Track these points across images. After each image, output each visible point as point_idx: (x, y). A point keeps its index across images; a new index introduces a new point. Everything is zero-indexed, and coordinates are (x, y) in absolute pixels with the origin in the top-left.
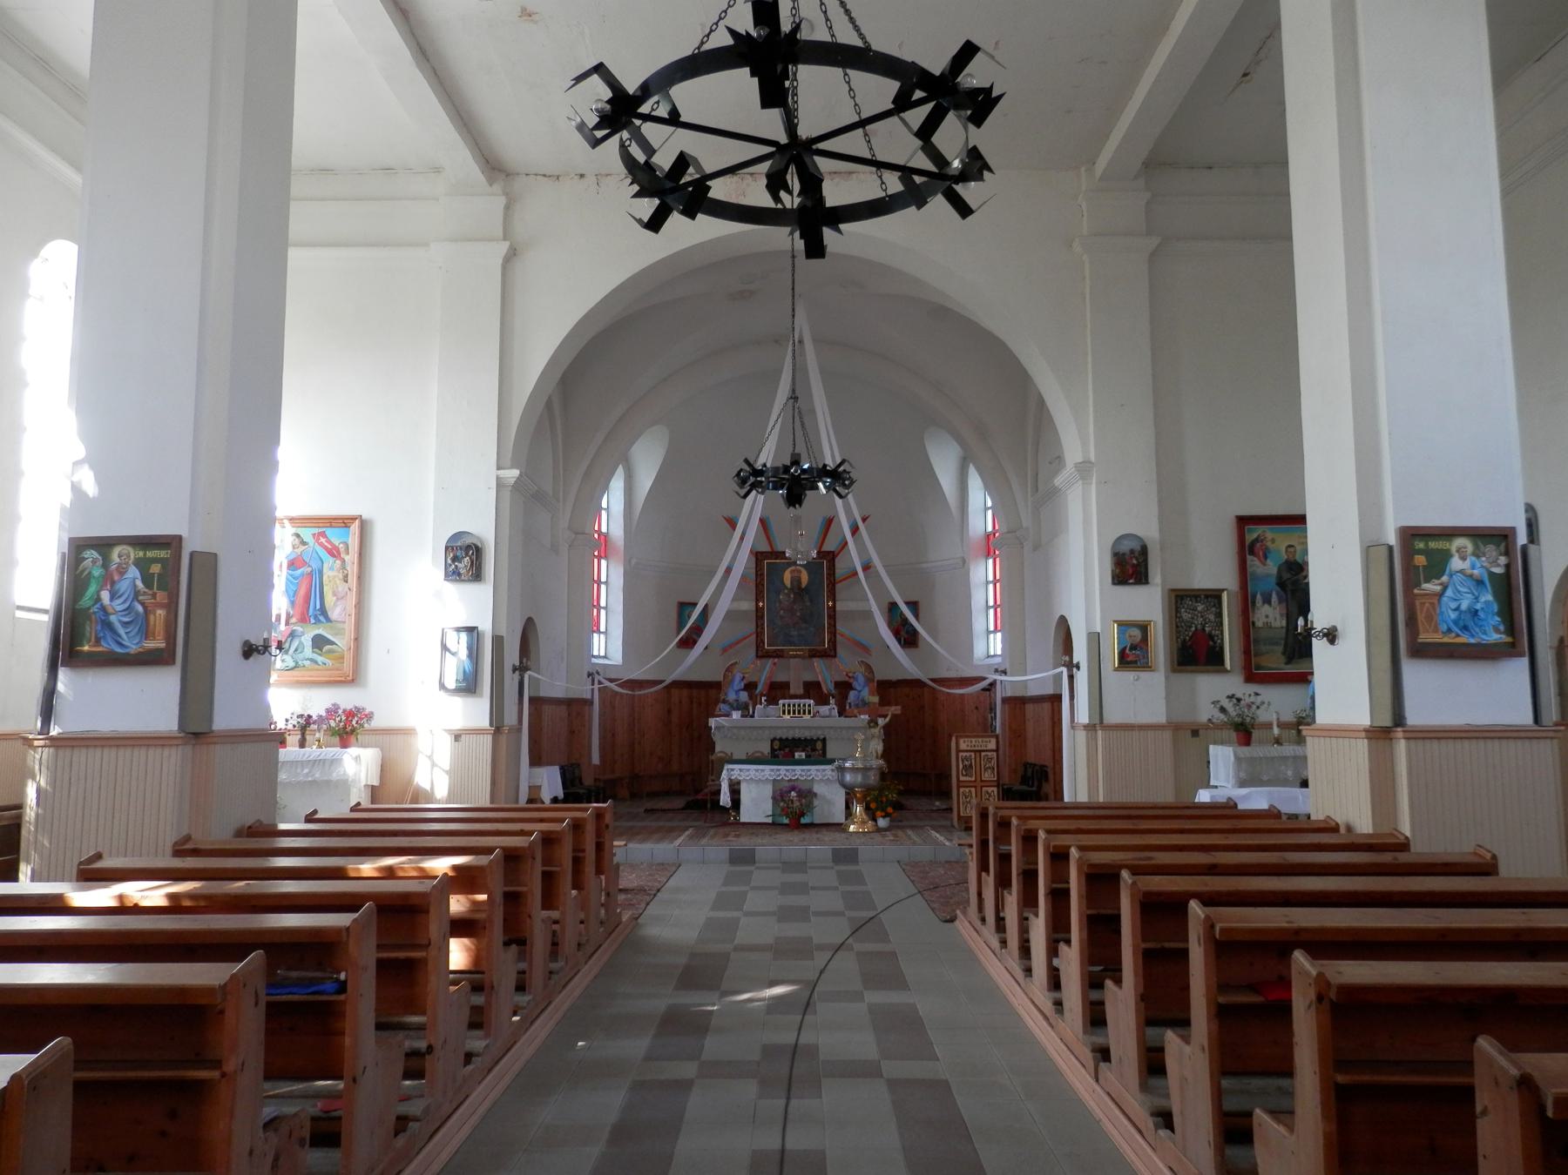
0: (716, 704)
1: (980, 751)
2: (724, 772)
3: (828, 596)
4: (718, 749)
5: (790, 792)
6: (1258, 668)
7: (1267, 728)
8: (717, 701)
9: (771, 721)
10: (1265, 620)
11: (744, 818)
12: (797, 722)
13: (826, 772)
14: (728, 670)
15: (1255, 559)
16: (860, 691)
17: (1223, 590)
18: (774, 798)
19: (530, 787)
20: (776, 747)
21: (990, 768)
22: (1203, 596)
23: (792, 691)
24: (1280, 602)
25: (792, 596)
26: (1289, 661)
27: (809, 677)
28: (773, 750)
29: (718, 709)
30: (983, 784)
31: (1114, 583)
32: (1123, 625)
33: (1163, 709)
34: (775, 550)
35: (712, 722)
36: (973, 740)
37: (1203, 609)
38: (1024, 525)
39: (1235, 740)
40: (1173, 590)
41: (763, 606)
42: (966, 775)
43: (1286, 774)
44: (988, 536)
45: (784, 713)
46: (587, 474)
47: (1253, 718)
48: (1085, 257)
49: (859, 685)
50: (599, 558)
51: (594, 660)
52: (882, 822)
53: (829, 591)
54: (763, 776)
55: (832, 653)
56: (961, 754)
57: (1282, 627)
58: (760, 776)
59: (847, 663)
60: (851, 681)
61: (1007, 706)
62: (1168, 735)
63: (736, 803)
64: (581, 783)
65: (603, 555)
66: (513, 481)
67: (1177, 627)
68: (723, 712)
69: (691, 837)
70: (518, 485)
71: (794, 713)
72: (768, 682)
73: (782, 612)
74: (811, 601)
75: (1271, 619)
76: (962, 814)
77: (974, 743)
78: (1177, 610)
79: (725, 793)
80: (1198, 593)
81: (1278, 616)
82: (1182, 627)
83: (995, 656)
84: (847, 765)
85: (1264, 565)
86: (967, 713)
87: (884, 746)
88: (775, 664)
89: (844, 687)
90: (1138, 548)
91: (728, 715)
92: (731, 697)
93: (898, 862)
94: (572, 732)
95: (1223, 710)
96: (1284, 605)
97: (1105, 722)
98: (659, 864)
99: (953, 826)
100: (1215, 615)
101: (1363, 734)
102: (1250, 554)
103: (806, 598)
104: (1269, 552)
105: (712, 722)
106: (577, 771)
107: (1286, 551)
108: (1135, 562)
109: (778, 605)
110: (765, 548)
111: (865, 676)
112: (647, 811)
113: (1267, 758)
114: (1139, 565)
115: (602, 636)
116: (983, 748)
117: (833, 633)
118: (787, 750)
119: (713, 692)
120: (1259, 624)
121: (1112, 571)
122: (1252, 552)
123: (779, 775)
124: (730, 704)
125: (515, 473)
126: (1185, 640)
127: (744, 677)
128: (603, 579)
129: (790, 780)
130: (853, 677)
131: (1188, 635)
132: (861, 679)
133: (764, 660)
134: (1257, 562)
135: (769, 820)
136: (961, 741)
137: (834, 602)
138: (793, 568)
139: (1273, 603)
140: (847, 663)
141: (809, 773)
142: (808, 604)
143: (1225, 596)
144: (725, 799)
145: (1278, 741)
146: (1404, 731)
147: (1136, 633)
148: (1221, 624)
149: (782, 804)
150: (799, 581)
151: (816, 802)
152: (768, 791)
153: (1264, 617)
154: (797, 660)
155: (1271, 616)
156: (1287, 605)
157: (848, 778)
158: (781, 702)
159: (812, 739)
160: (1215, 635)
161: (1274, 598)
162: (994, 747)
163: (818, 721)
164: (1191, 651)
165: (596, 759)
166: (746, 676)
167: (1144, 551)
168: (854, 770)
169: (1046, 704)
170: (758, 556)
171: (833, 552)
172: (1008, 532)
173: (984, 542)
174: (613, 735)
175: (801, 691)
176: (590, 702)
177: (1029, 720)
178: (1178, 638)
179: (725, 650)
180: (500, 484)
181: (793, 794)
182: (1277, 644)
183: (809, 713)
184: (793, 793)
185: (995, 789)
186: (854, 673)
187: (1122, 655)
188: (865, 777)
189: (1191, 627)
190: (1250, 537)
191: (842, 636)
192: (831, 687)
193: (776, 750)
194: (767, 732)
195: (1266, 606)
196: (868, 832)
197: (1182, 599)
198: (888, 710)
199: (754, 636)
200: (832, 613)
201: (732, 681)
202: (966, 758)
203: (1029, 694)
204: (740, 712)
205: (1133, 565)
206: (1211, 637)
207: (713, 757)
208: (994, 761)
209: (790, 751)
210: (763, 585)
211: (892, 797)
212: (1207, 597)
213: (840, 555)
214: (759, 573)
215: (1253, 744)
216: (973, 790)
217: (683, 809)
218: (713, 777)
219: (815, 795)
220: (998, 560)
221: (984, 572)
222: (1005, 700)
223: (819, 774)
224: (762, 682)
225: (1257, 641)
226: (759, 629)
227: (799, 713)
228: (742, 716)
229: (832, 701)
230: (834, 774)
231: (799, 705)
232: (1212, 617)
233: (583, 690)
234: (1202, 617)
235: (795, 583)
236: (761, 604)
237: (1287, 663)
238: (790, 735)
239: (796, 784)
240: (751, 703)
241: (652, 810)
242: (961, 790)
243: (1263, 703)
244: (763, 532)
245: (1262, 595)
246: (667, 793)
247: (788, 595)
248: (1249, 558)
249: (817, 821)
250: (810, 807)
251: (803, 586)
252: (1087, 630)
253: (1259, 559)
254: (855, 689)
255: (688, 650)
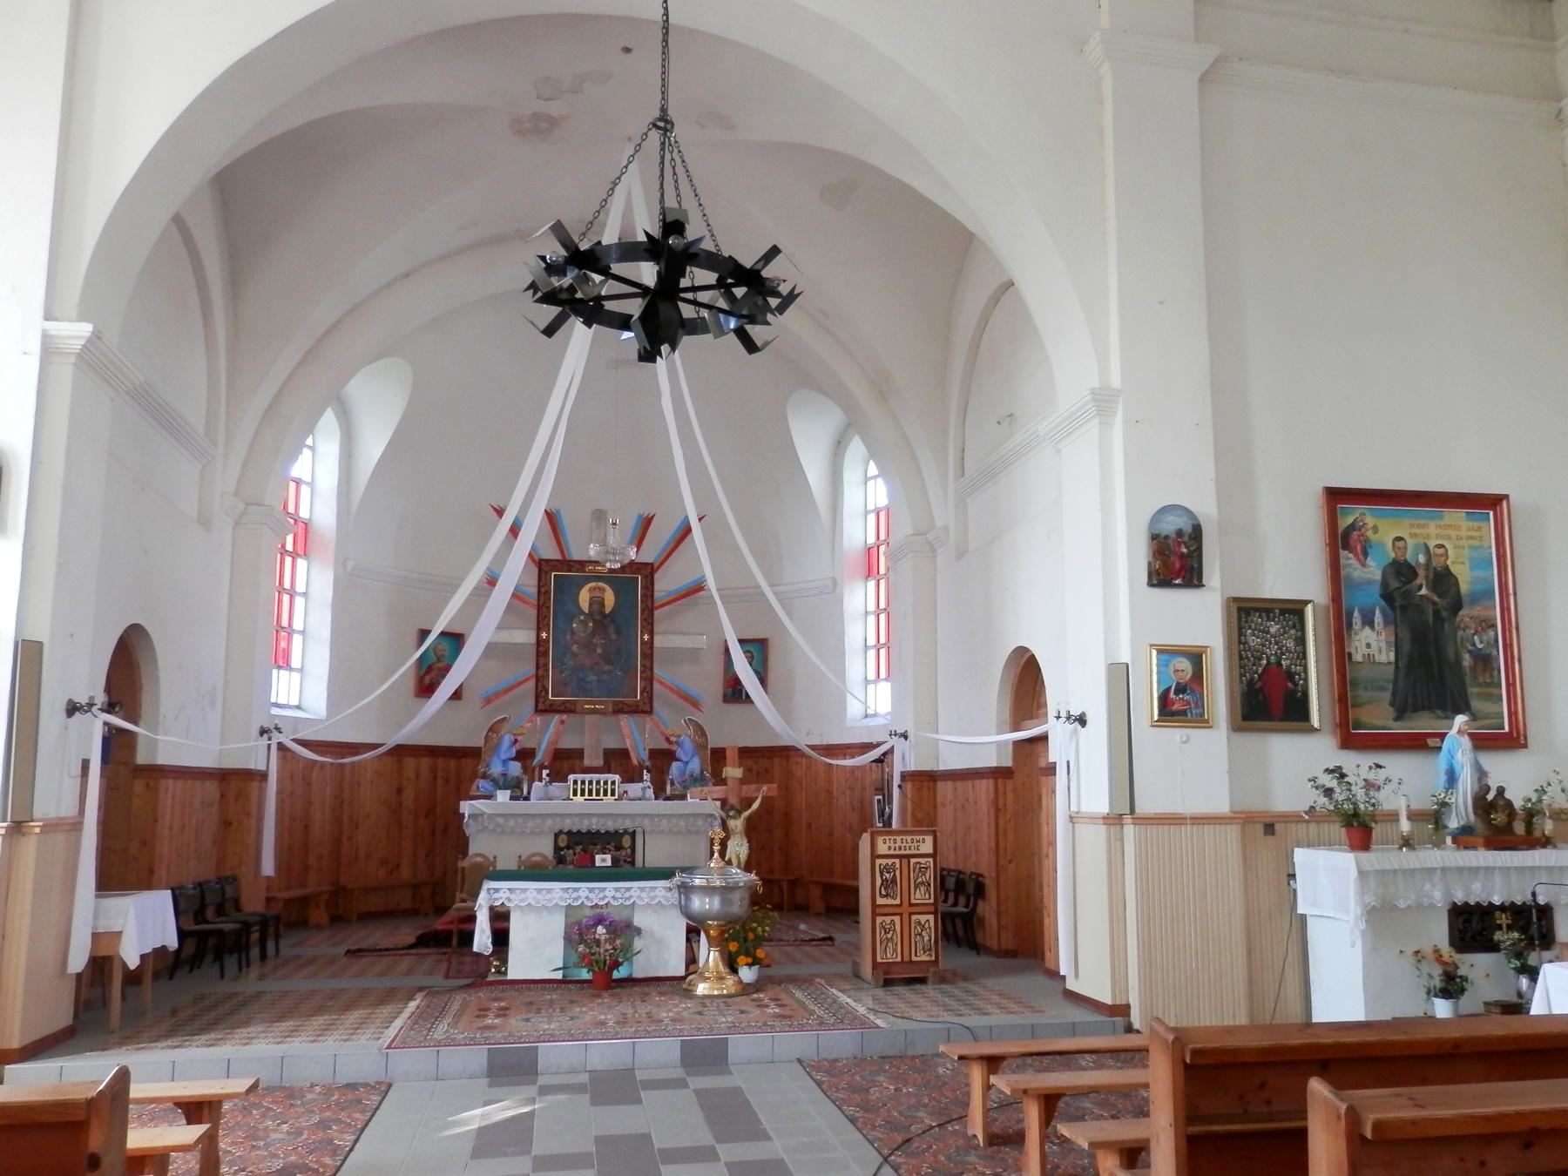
0: (472, 781)
1: (909, 857)
2: (483, 895)
3: (642, 627)
4: (473, 848)
5: (596, 925)
6: (1358, 725)
7: (1392, 821)
8: (474, 776)
9: (557, 806)
10: (1366, 651)
11: (515, 972)
12: (594, 808)
13: (657, 892)
14: (491, 729)
15: (1351, 555)
16: (687, 763)
17: (1307, 602)
18: (568, 938)
19: (94, 935)
20: (562, 845)
21: (922, 883)
22: (1277, 611)
23: (587, 762)
24: (1386, 623)
25: (591, 624)
26: (1401, 713)
27: (612, 743)
28: (557, 849)
29: (474, 787)
30: (913, 909)
31: (1151, 584)
32: (1166, 652)
33: (1226, 793)
34: (568, 558)
35: (466, 807)
36: (898, 839)
37: (1279, 630)
38: (939, 523)
39: (1344, 838)
40: (1236, 600)
41: (548, 637)
42: (886, 896)
43: (1432, 897)
44: (869, 549)
45: (575, 794)
46: (271, 410)
47: (1373, 805)
48: (1106, 70)
49: (685, 752)
50: (294, 555)
51: (275, 711)
52: (747, 974)
53: (644, 620)
54: (550, 900)
55: (647, 708)
56: (878, 861)
57: (1390, 663)
58: (543, 899)
59: (669, 720)
60: (674, 748)
61: (909, 786)
62: (1233, 832)
63: (501, 938)
64: (238, 908)
65: (301, 551)
66: (77, 345)
67: (1241, 658)
68: (482, 791)
69: (418, 1018)
70: (91, 357)
71: (590, 793)
72: (553, 747)
73: (575, 648)
74: (618, 631)
75: (1374, 650)
76: (879, 960)
77: (899, 843)
78: (1241, 633)
79: (483, 931)
80: (1269, 606)
81: (1383, 645)
82: (1247, 658)
83: (875, 715)
84: (697, 882)
85: (1364, 565)
86: (835, 794)
87: (750, 848)
88: (562, 722)
89: (662, 758)
90: (1188, 529)
91: (490, 797)
92: (496, 769)
93: (799, 1061)
94: (227, 824)
95: (1328, 792)
96: (1392, 628)
97: (1137, 810)
98: (348, 1086)
99: (857, 976)
100: (1296, 640)
101: (1101, 821)
102: (1344, 549)
103: (611, 629)
104: (1371, 547)
105: (466, 807)
106: (229, 889)
107: (1393, 545)
108: (1184, 550)
109: (568, 637)
110: (550, 552)
111: (693, 741)
112: (350, 953)
113: (1404, 871)
114: (1189, 555)
115: (296, 676)
116: (914, 852)
117: (649, 679)
118: (578, 849)
119: (467, 763)
120: (1358, 657)
121: (1149, 563)
122: (1346, 546)
123: (577, 899)
124: (492, 780)
125: (86, 329)
126: (1252, 678)
127: (516, 741)
128: (300, 587)
129: (596, 906)
130: (677, 743)
131: (1256, 672)
132: (688, 744)
133: (548, 717)
134: (1353, 562)
135: (559, 975)
136: (880, 840)
137: (651, 634)
138: (593, 584)
139: (1376, 626)
140: (669, 720)
141: (627, 895)
142: (613, 637)
143: (1309, 609)
144: (482, 940)
145: (1407, 843)
146: (1133, 818)
147: (1185, 665)
148: (1303, 655)
149: (581, 948)
150: (602, 605)
151: (638, 944)
152: (558, 924)
153: (1364, 646)
154: (596, 717)
155: (1374, 645)
156: (1396, 629)
157: (699, 904)
158: (571, 777)
159: (616, 832)
160: (1296, 673)
161: (1378, 618)
162: (930, 850)
163: (626, 807)
164: (1261, 697)
165: (268, 867)
166: (519, 738)
167: (1197, 532)
168: (709, 890)
169: (984, 781)
170: (542, 566)
171: (652, 564)
172: (915, 535)
173: (864, 559)
174: (306, 827)
175: (600, 762)
176: (263, 776)
177: (944, 805)
178: (1242, 675)
179: (488, 701)
180: (49, 349)
181: (601, 930)
182: (1382, 689)
183: (613, 794)
184: (600, 928)
185: (931, 918)
186: (679, 736)
187: (1164, 700)
188: (724, 902)
189: (1261, 659)
190: (1345, 522)
191: (661, 683)
192: (645, 755)
193: (562, 849)
194: (549, 822)
195: (1367, 630)
196: (729, 996)
197: (1248, 614)
198: (758, 790)
199: (532, 683)
200: (648, 651)
201: (497, 747)
202: (887, 869)
203: (942, 768)
204: (509, 792)
205: (1182, 556)
206: (1290, 676)
207: (465, 863)
208: (930, 874)
209: (584, 850)
210: (548, 608)
211: (764, 931)
212: (1283, 612)
213: (660, 570)
214: (543, 590)
215: (1374, 847)
216: (897, 919)
217: (412, 946)
218: (464, 896)
219: (638, 931)
220: (882, 583)
221: (860, 598)
222: (905, 776)
223: (644, 895)
224: (542, 750)
225: (1355, 683)
226: (540, 672)
227: (598, 794)
228: (512, 798)
229: (646, 776)
230: (669, 894)
231: (598, 783)
232: (1290, 644)
233: (254, 755)
234: (1276, 643)
235: (595, 607)
236: (544, 635)
237: (1397, 719)
238: (584, 826)
239: (605, 911)
240: (526, 778)
241: (360, 950)
242: (879, 920)
243: (1388, 780)
244: (552, 535)
245: (1361, 611)
246: (389, 915)
247: (584, 623)
248: (1343, 553)
249: (638, 974)
250: (627, 952)
251: (608, 610)
252: (1106, 658)
253: (1356, 556)
254: (681, 760)
255: (424, 699)
